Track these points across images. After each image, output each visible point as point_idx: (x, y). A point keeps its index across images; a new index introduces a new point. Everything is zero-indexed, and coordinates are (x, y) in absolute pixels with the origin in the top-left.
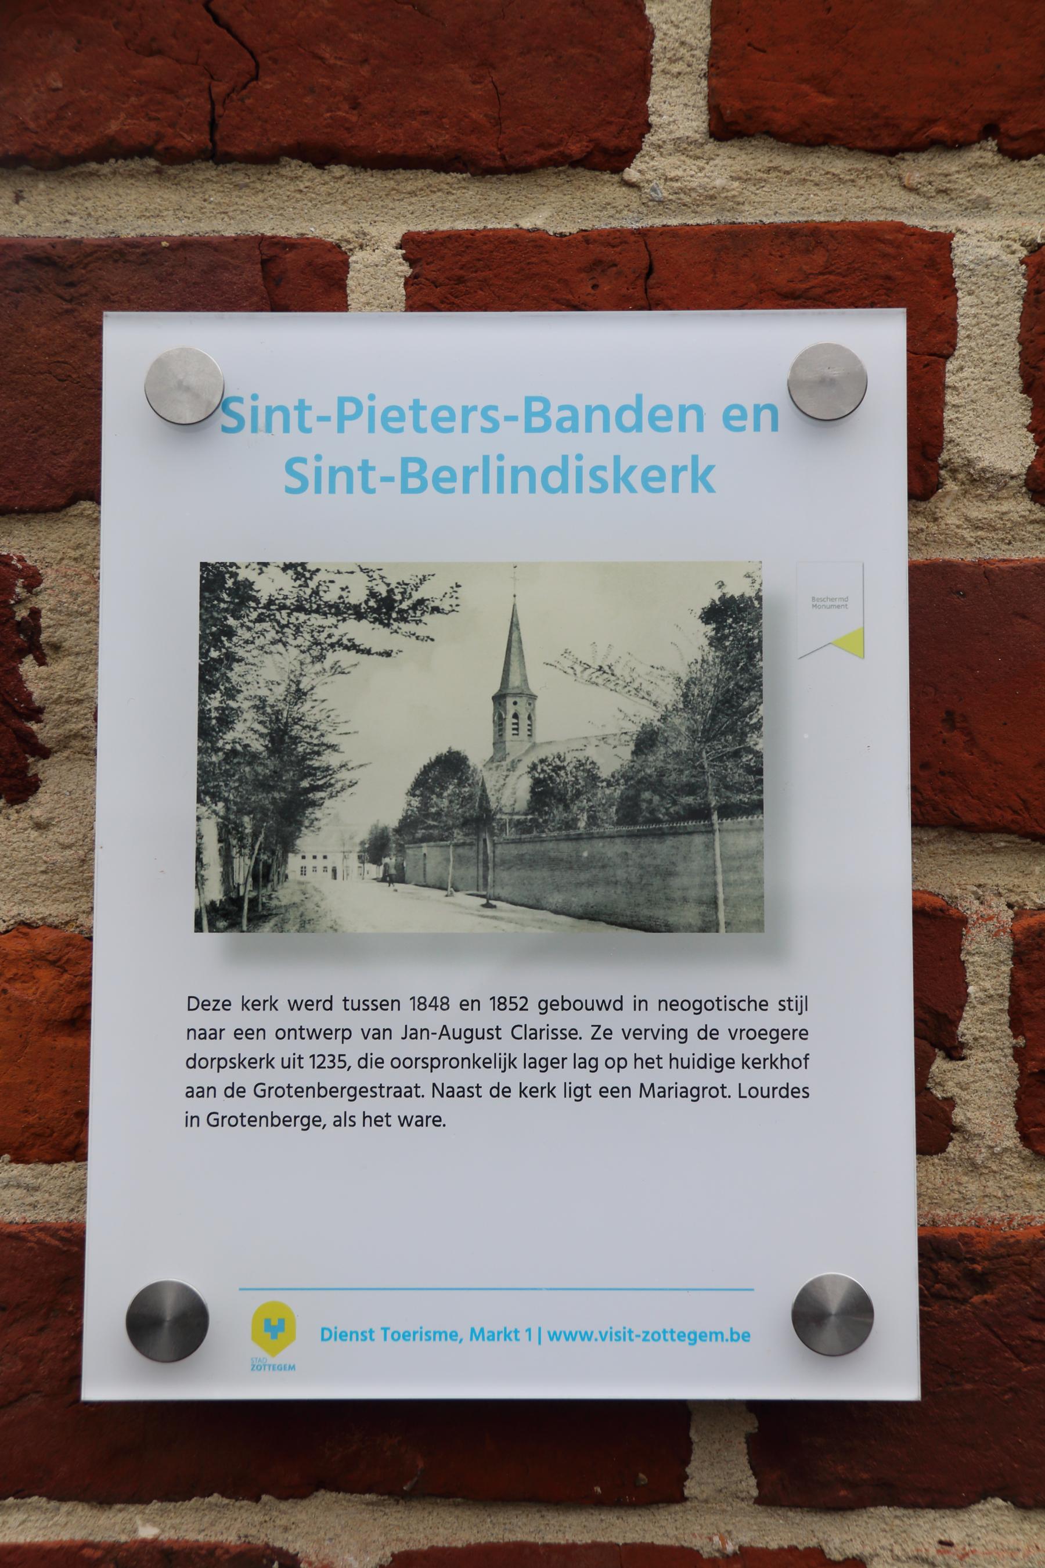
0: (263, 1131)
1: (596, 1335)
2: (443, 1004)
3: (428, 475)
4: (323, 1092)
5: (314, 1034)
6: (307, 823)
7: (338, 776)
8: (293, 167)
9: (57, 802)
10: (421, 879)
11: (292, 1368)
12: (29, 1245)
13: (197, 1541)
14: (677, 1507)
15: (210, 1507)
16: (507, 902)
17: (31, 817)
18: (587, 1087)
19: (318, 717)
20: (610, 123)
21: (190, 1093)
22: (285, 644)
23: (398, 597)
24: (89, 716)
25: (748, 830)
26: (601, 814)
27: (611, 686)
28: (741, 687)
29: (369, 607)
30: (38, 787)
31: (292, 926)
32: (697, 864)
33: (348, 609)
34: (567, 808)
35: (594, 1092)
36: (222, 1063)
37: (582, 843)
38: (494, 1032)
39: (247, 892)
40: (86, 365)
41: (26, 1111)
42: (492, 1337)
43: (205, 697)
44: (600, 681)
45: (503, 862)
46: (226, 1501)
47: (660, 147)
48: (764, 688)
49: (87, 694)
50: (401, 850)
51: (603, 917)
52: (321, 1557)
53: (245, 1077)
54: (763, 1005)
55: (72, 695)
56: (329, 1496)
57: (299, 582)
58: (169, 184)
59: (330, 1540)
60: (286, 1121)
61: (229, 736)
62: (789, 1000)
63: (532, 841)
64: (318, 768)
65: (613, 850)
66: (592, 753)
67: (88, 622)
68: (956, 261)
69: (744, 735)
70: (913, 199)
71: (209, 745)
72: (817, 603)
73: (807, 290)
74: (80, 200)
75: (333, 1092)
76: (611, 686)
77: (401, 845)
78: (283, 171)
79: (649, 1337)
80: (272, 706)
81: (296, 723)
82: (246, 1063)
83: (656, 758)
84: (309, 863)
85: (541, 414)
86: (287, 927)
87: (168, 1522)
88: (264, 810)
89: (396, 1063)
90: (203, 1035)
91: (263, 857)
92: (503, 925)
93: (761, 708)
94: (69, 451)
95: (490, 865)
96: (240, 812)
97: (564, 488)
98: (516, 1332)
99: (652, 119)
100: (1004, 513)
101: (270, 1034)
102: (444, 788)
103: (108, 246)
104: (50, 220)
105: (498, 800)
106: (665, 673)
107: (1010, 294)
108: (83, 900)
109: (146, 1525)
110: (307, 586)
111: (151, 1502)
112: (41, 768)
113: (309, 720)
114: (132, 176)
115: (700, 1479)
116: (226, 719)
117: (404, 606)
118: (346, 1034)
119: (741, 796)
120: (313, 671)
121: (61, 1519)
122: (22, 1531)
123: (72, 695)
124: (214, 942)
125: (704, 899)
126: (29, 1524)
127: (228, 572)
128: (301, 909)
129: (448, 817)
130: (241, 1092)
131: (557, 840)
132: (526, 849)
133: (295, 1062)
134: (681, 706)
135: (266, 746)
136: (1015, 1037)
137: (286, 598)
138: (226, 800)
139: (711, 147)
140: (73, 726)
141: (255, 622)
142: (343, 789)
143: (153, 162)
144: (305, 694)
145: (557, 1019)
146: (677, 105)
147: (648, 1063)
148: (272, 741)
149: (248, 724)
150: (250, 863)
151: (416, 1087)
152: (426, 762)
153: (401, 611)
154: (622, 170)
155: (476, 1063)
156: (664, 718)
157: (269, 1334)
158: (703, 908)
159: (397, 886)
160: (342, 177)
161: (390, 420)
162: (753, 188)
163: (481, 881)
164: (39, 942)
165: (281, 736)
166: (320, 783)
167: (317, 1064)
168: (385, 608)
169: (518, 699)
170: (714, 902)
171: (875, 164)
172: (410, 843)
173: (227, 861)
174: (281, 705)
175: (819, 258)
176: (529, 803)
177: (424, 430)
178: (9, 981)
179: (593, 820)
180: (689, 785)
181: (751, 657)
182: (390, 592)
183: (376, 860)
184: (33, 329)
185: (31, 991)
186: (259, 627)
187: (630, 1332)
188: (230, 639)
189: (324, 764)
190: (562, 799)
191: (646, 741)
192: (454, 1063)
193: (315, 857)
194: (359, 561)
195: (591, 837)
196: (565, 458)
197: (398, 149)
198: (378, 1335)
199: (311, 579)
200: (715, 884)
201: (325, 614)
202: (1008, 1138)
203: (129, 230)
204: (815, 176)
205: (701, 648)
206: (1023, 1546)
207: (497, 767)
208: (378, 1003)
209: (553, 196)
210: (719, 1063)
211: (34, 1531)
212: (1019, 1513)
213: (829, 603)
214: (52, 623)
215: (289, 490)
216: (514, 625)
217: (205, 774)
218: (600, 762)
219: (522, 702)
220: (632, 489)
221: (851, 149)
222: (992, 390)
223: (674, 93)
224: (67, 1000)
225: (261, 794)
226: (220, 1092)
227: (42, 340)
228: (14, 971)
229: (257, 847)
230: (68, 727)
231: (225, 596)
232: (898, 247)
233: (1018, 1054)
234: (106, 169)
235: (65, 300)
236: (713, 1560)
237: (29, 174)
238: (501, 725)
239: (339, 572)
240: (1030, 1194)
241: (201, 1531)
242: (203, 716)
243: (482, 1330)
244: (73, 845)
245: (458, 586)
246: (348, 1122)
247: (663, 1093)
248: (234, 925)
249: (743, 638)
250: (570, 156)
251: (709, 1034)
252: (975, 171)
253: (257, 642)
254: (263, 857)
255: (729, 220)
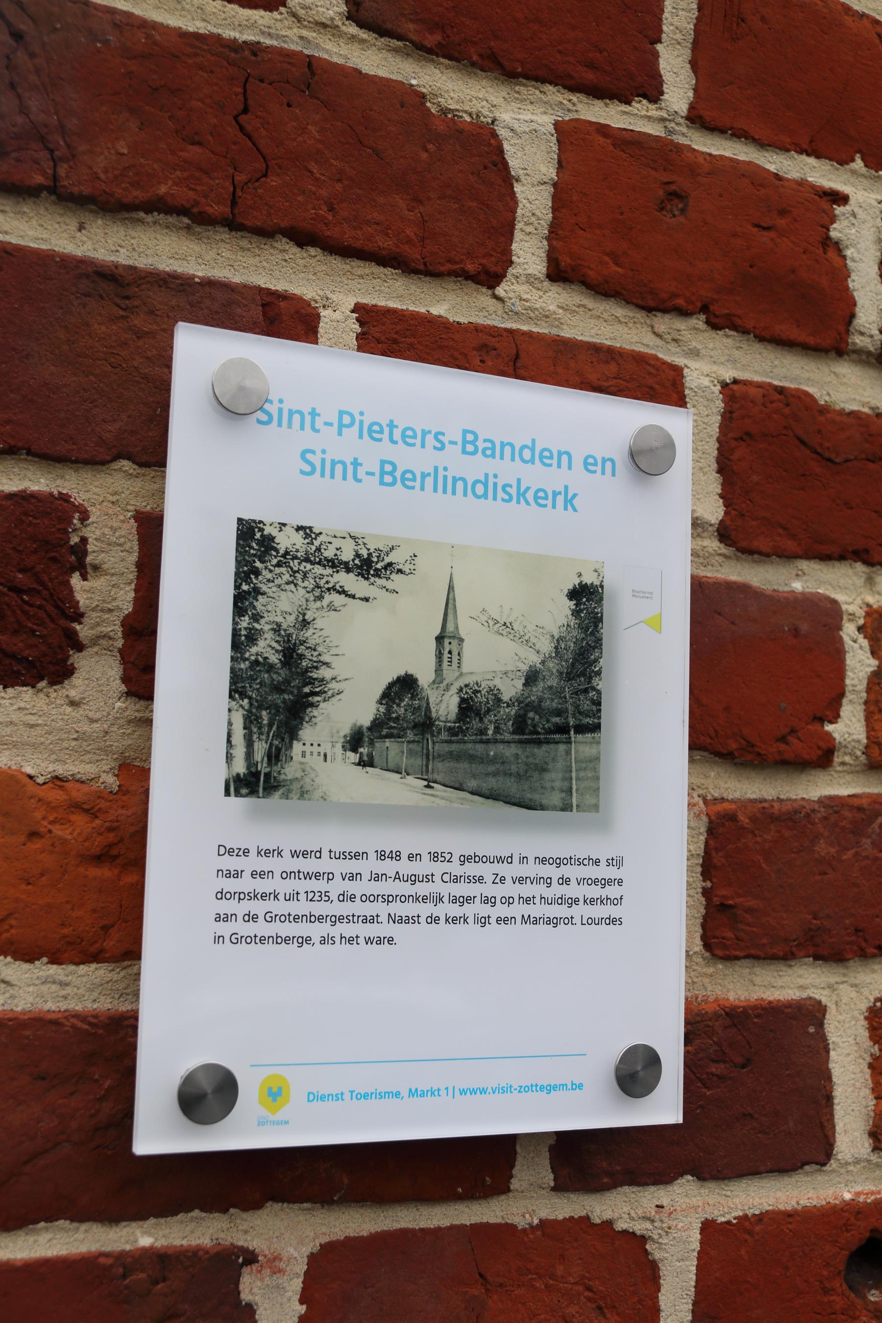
0: (270, 947)
1: (489, 1090)
2: (398, 856)
3: (398, 474)
4: (313, 919)
5: (308, 876)
6: (307, 719)
7: (330, 686)
8: (283, 243)
9: (88, 686)
10: (385, 765)
11: (287, 1122)
12: (66, 1028)
13: (182, 1245)
14: (503, 1197)
15: (192, 1219)
16: (441, 784)
17: (67, 696)
18: (489, 917)
19: (317, 641)
20: (491, 255)
21: (218, 918)
22: (296, 585)
23: (375, 559)
24: (117, 622)
25: (591, 743)
26: (502, 726)
27: (511, 637)
28: (589, 645)
29: (355, 564)
30: (73, 673)
31: (294, 795)
32: (560, 764)
33: (341, 564)
34: (481, 720)
35: (493, 920)
36: (242, 896)
37: (490, 745)
38: (430, 877)
39: (263, 768)
40: (133, 359)
41: (63, 925)
42: (423, 1094)
43: (237, 619)
44: (504, 633)
45: (439, 756)
46: (204, 1214)
47: (517, 277)
48: (603, 647)
49: (117, 606)
50: (372, 743)
51: (502, 798)
52: (272, 1251)
53: (258, 907)
54: (597, 862)
55: (105, 605)
56: (277, 1206)
57: (307, 541)
58: (193, 238)
59: (277, 1237)
60: (287, 940)
61: (254, 650)
62: (613, 859)
63: (458, 742)
64: (316, 679)
65: (510, 751)
66: (498, 682)
67: (122, 551)
68: (687, 385)
69: (591, 678)
70: (658, 342)
71: (239, 655)
72: (635, 594)
73: (608, 387)
74: (128, 238)
75: (320, 919)
76: (511, 637)
77: (372, 740)
78: (276, 244)
79: (522, 1090)
80: (285, 630)
81: (302, 644)
82: (259, 896)
83: (538, 689)
84: (308, 749)
85: (473, 443)
86: (291, 795)
87: (161, 1233)
88: (277, 707)
89: (364, 898)
90: (229, 875)
91: (276, 742)
92: (437, 801)
93: (601, 660)
94: (115, 420)
95: (431, 757)
96: (260, 707)
97: (485, 495)
98: (439, 1090)
99: (514, 258)
100: (705, 547)
101: (277, 875)
102: (402, 700)
103: (157, 274)
104: (105, 248)
105: (437, 711)
106: (545, 632)
107: (714, 411)
108: (104, 762)
109: (142, 1237)
110: (313, 544)
111: (148, 1218)
112: (78, 659)
113: (311, 643)
114: (167, 227)
115: (520, 1178)
116: (252, 637)
117: (379, 566)
118: (330, 877)
119: (588, 720)
120: (315, 607)
121: (80, 1236)
122: (50, 1247)
123: (105, 605)
124: (238, 804)
125: (564, 788)
126: (55, 1241)
127: (257, 527)
128: (302, 783)
129: (402, 724)
130: (255, 918)
131: (475, 742)
132: (454, 747)
133: (293, 896)
134: (554, 655)
135: (280, 660)
136: (704, 881)
137: (297, 551)
138: (250, 698)
139: (547, 284)
140: (104, 629)
141: (275, 566)
142: (333, 696)
143: (186, 220)
144: (309, 623)
145: (471, 869)
146: (529, 253)
147: (527, 901)
148: (284, 656)
149: (267, 642)
150: (266, 746)
151: (377, 916)
152: (390, 680)
153: (376, 570)
154: (495, 288)
155: (417, 899)
156: (543, 662)
157: (271, 1099)
158: (563, 795)
159: (368, 769)
160: (316, 256)
161: (374, 432)
162: (569, 316)
163: (424, 768)
164: (74, 794)
165: (291, 653)
166: (317, 690)
167: (309, 898)
168: (366, 567)
169: (452, 641)
170: (570, 791)
171: (640, 315)
172: (378, 738)
173: (249, 744)
174: (291, 630)
175: (613, 368)
176: (457, 715)
177: (396, 443)
178: (51, 823)
179: (497, 730)
180: (557, 709)
181: (596, 626)
182: (370, 555)
183: (354, 750)
184: (96, 326)
185: (68, 832)
186: (278, 570)
187: (511, 1087)
188: (257, 578)
189: (321, 676)
190: (478, 714)
191: (532, 677)
192: (403, 899)
193: (312, 745)
194: (349, 530)
195: (496, 741)
196: (487, 475)
197: (358, 245)
198: (347, 1096)
199: (316, 539)
200: (571, 778)
201: (324, 566)
202: (697, 945)
203: (166, 265)
204: (605, 315)
205: (567, 616)
206: (700, 1203)
207: (437, 688)
208: (352, 854)
209: (450, 296)
210: (570, 901)
211: (59, 1246)
212: (700, 1183)
213: (642, 595)
214: (96, 549)
215: (302, 472)
216: (451, 588)
217: (236, 678)
218: (503, 689)
219: (455, 642)
220: (528, 503)
221: (628, 303)
222: (701, 469)
223: (526, 244)
224: (98, 840)
225: (276, 693)
226: (240, 918)
227: (102, 335)
228: (55, 815)
229: (271, 735)
230: (99, 629)
231: (254, 545)
232: (657, 370)
233: (705, 892)
234: (149, 219)
235: (122, 309)
236: (524, 1230)
237: (92, 211)
238: (440, 658)
239: (335, 537)
240: (706, 981)
241: (183, 1238)
242: (235, 633)
243: (416, 1090)
244: (99, 720)
245: (415, 556)
246: (330, 941)
247: (536, 922)
248: (253, 792)
249: (592, 613)
250: (468, 272)
251: (565, 881)
252: (692, 330)
253: (276, 581)
254: (276, 742)
255: (556, 333)
